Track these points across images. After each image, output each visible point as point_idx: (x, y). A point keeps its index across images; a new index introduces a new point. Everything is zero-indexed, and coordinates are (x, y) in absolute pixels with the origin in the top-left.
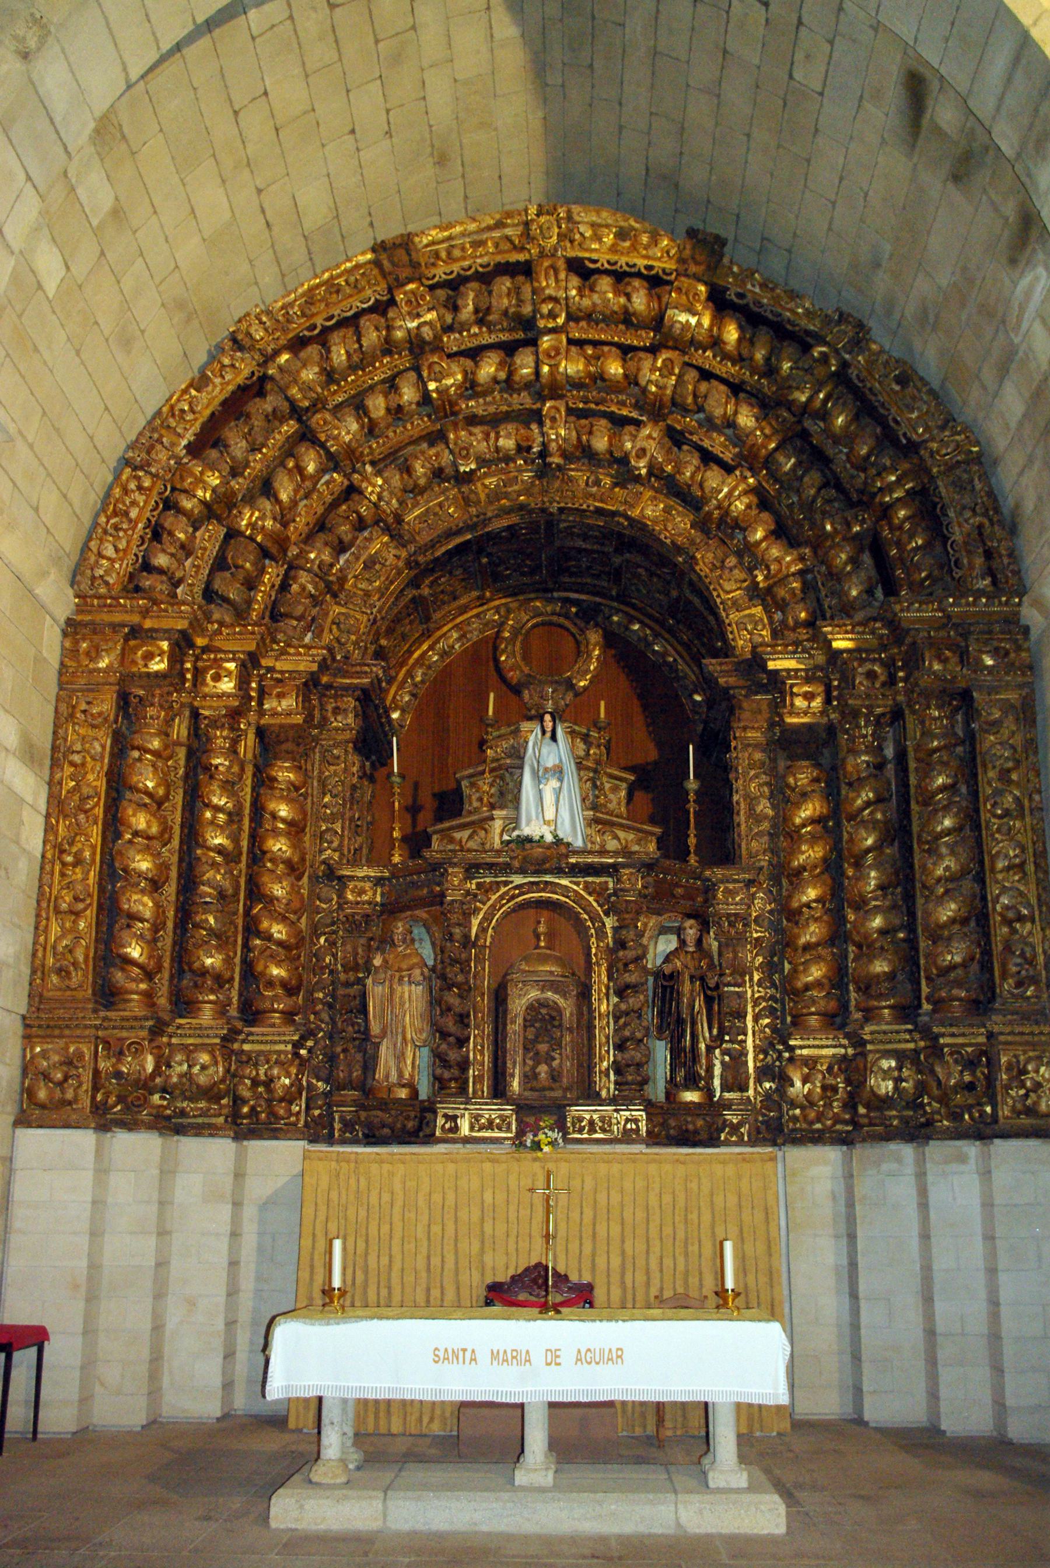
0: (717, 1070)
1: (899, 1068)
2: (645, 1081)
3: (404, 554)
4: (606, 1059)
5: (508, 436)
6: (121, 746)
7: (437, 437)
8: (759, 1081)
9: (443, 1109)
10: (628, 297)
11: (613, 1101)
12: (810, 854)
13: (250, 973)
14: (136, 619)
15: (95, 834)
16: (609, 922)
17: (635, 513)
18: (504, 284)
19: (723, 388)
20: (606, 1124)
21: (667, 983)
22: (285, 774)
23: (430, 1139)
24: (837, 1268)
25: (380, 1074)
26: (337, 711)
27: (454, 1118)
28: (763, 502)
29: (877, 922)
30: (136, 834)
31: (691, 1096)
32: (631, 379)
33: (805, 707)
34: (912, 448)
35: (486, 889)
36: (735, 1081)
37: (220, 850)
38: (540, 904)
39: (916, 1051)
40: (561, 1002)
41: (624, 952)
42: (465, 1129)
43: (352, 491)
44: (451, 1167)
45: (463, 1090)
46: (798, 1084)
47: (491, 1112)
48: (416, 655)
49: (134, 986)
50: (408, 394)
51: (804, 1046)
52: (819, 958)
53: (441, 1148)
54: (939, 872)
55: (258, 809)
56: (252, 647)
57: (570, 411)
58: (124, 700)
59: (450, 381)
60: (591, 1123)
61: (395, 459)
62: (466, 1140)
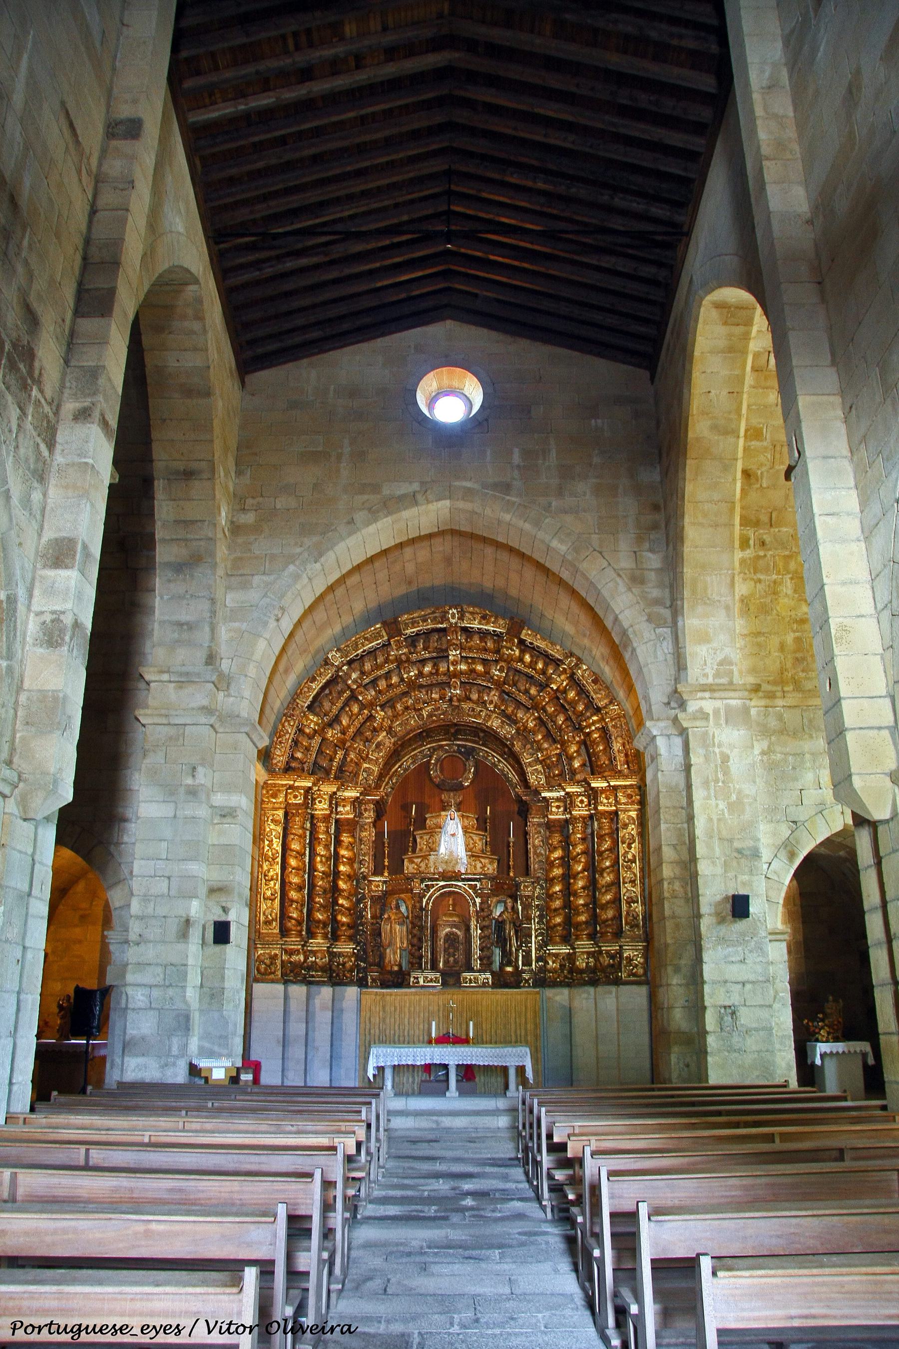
0: (520, 958)
1: (588, 958)
2: (491, 963)
3: (393, 740)
4: (476, 953)
5: (436, 693)
8: (537, 961)
9: (413, 974)
10: (486, 643)
11: (479, 971)
12: (557, 872)
13: (334, 920)
14: (292, 783)
15: (278, 868)
16: (478, 900)
17: (489, 724)
18: (436, 636)
19: (525, 678)
20: (476, 979)
21: (500, 924)
22: (346, 838)
25: (387, 961)
26: (366, 810)
27: (417, 978)
28: (541, 722)
29: (581, 902)
30: (293, 869)
31: (509, 969)
32: (487, 672)
33: (557, 814)
34: (598, 710)
35: (433, 886)
36: (527, 962)
38: (450, 892)
39: (594, 952)
40: (459, 933)
41: (485, 909)
42: (422, 983)
43: (371, 718)
44: (417, 997)
45: (420, 967)
46: (551, 963)
47: (431, 975)
48: (393, 770)
49: (294, 928)
50: (395, 680)
51: (553, 949)
52: (560, 914)
53: (413, 990)
54: (604, 882)
56: (335, 790)
57: (461, 682)
58: (286, 814)
59: (412, 674)
60: (470, 980)
61: (389, 704)
62: (423, 987)
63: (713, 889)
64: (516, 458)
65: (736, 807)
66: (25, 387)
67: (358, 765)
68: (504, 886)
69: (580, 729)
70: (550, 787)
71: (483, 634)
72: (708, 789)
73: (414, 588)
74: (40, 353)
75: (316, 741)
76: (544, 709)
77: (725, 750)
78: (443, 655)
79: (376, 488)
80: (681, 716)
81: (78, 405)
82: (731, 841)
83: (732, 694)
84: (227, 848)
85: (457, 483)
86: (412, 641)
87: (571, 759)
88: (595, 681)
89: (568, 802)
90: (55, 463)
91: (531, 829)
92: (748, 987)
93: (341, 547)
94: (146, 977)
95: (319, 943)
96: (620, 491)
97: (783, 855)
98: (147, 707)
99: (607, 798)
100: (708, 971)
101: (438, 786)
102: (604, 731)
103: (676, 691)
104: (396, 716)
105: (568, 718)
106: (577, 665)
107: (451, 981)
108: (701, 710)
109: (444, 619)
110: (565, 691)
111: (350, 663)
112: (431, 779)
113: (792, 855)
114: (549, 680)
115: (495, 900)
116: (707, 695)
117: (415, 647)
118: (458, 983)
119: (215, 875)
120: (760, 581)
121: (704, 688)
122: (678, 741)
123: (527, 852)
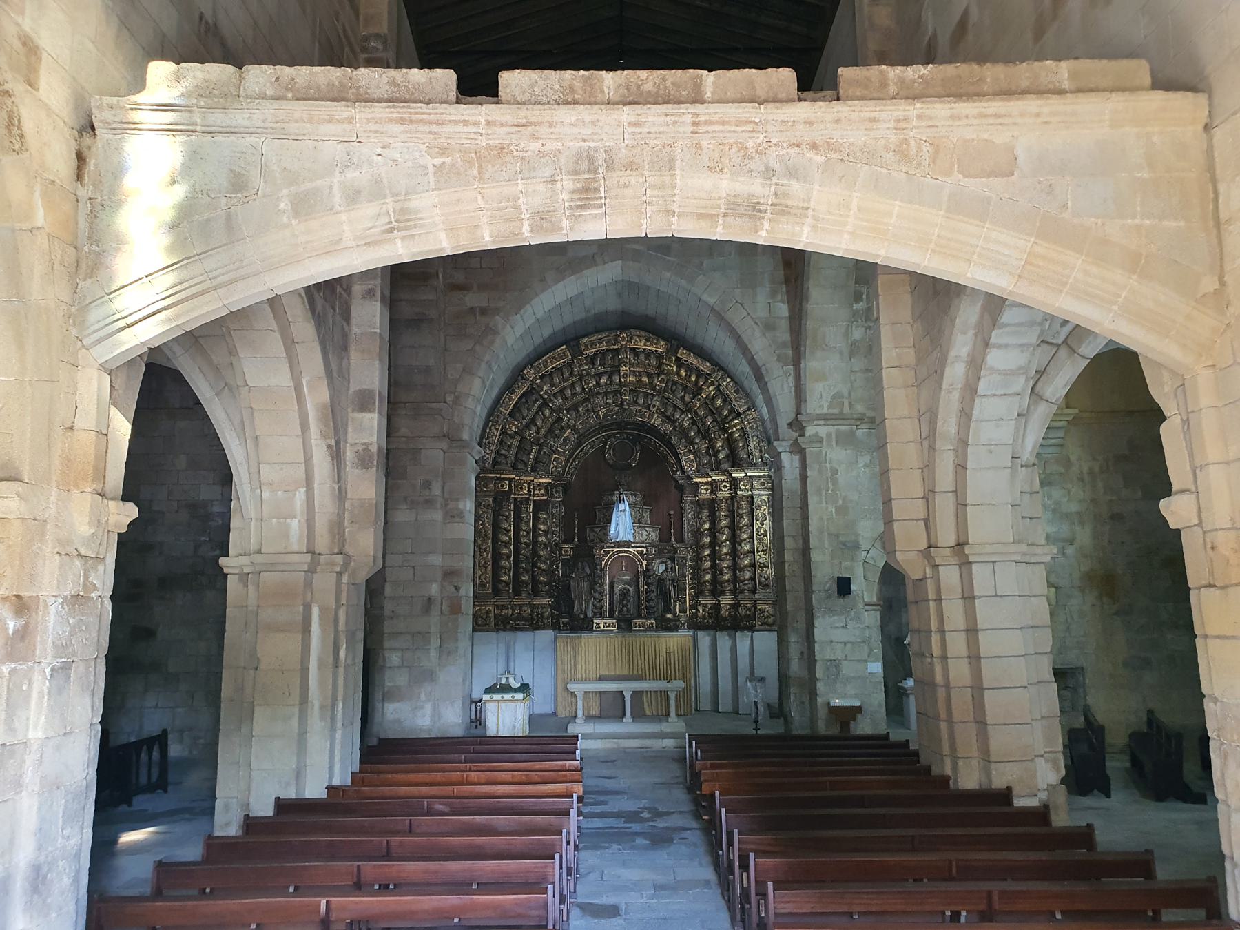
11: (645, 618)
15: (490, 542)
16: (644, 562)
21: (661, 581)
22: (543, 516)
23: (591, 630)
28: (694, 423)
31: (669, 616)
33: (705, 495)
34: (739, 414)
41: (648, 573)
43: (559, 419)
47: (609, 622)
63: (825, 567)
67: (550, 456)
68: (664, 547)
69: (724, 429)
70: (700, 473)
71: (648, 354)
72: (821, 495)
75: (517, 439)
77: (835, 465)
78: (615, 370)
80: (800, 439)
81: (366, 288)
82: (837, 536)
86: (592, 360)
88: (737, 392)
89: (714, 486)
91: (686, 506)
92: (849, 646)
95: (522, 599)
97: (878, 545)
100: (818, 634)
101: (611, 466)
102: (743, 430)
103: (797, 419)
104: (579, 416)
108: (817, 434)
109: (616, 341)
111: (542, 377)
116: (822, 422)
122: (797, 458)
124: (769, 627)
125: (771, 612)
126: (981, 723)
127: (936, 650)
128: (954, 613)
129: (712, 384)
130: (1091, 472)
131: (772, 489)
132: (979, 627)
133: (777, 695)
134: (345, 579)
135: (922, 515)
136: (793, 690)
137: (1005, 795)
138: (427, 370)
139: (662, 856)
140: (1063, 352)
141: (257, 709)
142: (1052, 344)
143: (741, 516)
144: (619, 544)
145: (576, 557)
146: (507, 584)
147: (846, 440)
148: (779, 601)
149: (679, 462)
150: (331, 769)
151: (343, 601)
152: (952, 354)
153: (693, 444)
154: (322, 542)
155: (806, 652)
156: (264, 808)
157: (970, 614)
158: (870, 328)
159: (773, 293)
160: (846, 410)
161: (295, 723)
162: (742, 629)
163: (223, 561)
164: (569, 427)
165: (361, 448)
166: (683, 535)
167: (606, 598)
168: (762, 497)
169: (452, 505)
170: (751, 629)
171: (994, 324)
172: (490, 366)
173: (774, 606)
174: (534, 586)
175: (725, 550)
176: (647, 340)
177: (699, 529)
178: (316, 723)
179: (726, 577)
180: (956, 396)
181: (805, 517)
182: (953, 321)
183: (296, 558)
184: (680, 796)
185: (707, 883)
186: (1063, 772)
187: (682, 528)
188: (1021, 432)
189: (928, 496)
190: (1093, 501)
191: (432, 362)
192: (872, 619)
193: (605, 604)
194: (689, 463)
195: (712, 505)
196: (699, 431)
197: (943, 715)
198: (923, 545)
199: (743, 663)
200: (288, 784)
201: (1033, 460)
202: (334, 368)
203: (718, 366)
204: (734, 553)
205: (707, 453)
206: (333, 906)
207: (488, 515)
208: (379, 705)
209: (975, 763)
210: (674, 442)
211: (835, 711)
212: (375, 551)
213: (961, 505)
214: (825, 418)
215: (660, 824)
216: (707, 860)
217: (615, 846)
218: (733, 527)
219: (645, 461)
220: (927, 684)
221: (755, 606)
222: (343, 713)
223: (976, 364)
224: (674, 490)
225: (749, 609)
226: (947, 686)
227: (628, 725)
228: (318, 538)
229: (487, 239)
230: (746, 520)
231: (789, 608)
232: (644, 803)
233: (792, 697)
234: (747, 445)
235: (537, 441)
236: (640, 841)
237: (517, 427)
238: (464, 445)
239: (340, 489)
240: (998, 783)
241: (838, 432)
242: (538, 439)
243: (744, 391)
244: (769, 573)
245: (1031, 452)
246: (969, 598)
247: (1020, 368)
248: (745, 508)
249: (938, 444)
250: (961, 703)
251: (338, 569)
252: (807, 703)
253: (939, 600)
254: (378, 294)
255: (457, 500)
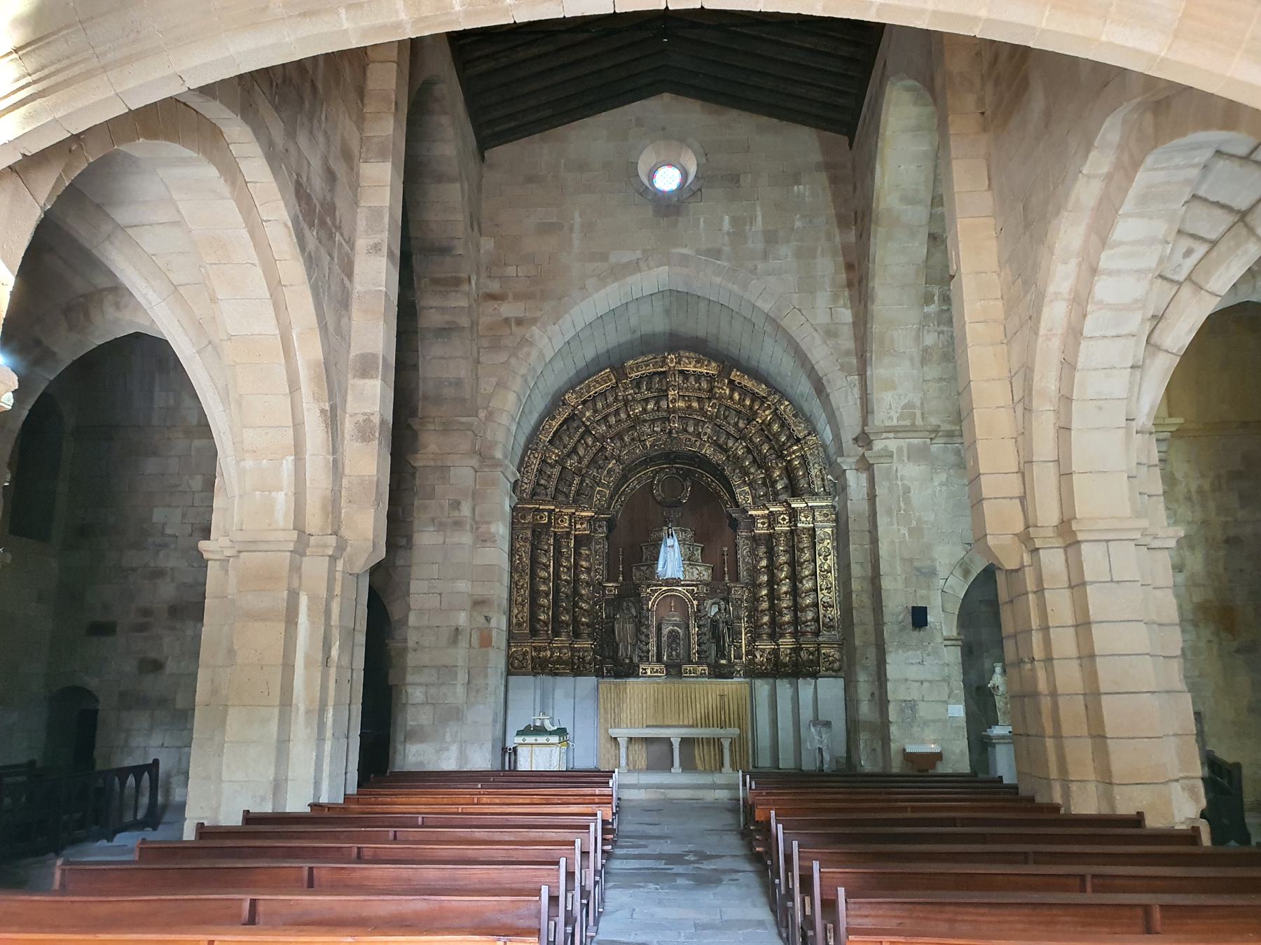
6: (534, 548)
7: (633, 428)
9: (641, 666)
15: (527, 578)
16: (695, 603)
21: (714, 622)
22: (584, 551)
23: (638, 676)
24: (1241, 166)
28: (749, 451)
31: (723, 662)
32: (702, 409)
33: (761, 529)
34: (798, 440)
35: (656, 591)
36: (739, 657)
37: (566, 581)
41: (699, 614)
43: (603, 449)
50: (623, 416)
55: (576, 564)
63: (897, 599)
64: (726, 225)
65: (916, 532)
66: (331, 237)
68: (717, 588)
70: (756, 506)
71: (698, 377)
73: (638, 334)
74: (339, 204)
75: (556, 471)
76: (751, 439)
79: (604, 257)
82: (911, 560)
83: (914, 435)
84: (489, 567)
85: (675, 250)
86: (637, 383)
87: (774, 482)
88: (795, 416)
89: (772, 519)
90: (355, 292)
91: (741, 542)
92: (926, 684)
93: (575, 311)
94: (423, 678)
96: (819, 252)
97: (958, 572)
98: (291, 134)
99: (806, 517)
100: (892, 671)
101: (659, 503)
102: (803, 458)
103: (863, 432)
105: (772, 448)
106: (779, 401)
107: (672, 671)
109: (664, 363)
110: (770, 424)
111: (584, 403)
112: (654, 498)
113: (966, 573)
114: (755, 413)
115: (710, 602)
116: (892, 435)
117: (639, 388)
118: (679, 674)
119: (480, 591)
120: (942, 332)
121: (889, 430)
122: (864, 477)
123: (737, 561)
124: (835, 673)
125: (837, 656)
126: (1099, 737)
127: (1038, 652)
128: (1060, 606)
129: (769, 407)
130: (1200, 491)
131: (836, 520)
132: (1092, 618)
133: (844, 748)
134: (340, 565)
135: (1018, 491)
136: (863, 737)
137: (1137, 820)
138: (458, 383)
139: (708, 897)
140: (1186, 291)
141: (231, 711)
142: (1172, 281)
143: (802, 550)
144: (668, 582)
145: (620, 597)
146: (546, 624)
147: (919, 454)
148: (846, 644)
149: (732, 495)
150: (317, 784)
151: (338, 591)
152: (1051, 289)
153: (747, 474)
154: (314, 520)
155: (877, 693)
156: (232, 818)
157: (1081, 606)
158: (942, 332)
159: (835, 297)
160: (919, 422)
161: (273, 728)
162: (805, 676)
163: (203, 545)
164: (613, 457)
165: (361, 418)
166: (737, 574)
167: (653, 641)
168: (825, 530)
169: (483, 528)
170: (815, 675)
171: (1104, 243)
172: (526, 381)
173: (840, 650)
174: (575, 624)
175: (784, 589)
176: (698, 362)
177: (755, 567)
178: (301, 730)
179: (787, 618)
180: (1056, 344)
181: (874, 541)
182: (1051, 250)
183: (280, 536)
184: (733, 843)
185: (761, 923)
186: (1204, 803)
187: (737, 566)
188: (1136, 389)
189: (1024, 472)
190: (1205, 523)
191: (463, 374)
192: (953, 655)
193: (653, 649)
194: (744, 495)
195: (770, 540)
196: (754, 461)
197: (1049, 730)
198: (1019, 527)
199: (806, 714)
200: (263, 799)
201: (1149, 425)
202: (330, 320)
203: (774, 389)
204: (795, 592)
205: (764, 484)
206: (261, 908)
207: (525, 549)
208: (400, 747)
209: (1091, 787)
210: (727, 473)
211: (909, 758)
212: (375, 536)
213: (1065, 476)
214: (895, 430)
215: (707, 866)
216: (763, 900)
217: (652, 886)
218: (794, 564)
219: (694, 491)
220: (1025, 697)
221: (818, 650)
222: (334, 721)
223: (1080, 302)
224: (728, 528)
225: (812, 654)
226: (1054, 694)
227: (677, 776)
228: (309, 518)
229: (457, 8)
230: (807, 555)
231: (857, 643)
232: (690, 847)
233: (862, 745)
234: (807, 473)
235: (578, 472)
236: (680, 881)
237: (557, 455)
238: (497, 464)
239: (335, 462)
240: (1125, 808)
241: (909, 445)
242: (580, 469)
243: (804, 415)
244: (834, 613)
245: (1148, 415)
246: (1078, 586)
247: (1136, 301)
248: (806, 542)
249: (1036, 404)
250: (1072, 713)
251: (330, 553)
252: (879, 749)
253: (1040, 591)
254: (385, 249)
255: (489, 523)
